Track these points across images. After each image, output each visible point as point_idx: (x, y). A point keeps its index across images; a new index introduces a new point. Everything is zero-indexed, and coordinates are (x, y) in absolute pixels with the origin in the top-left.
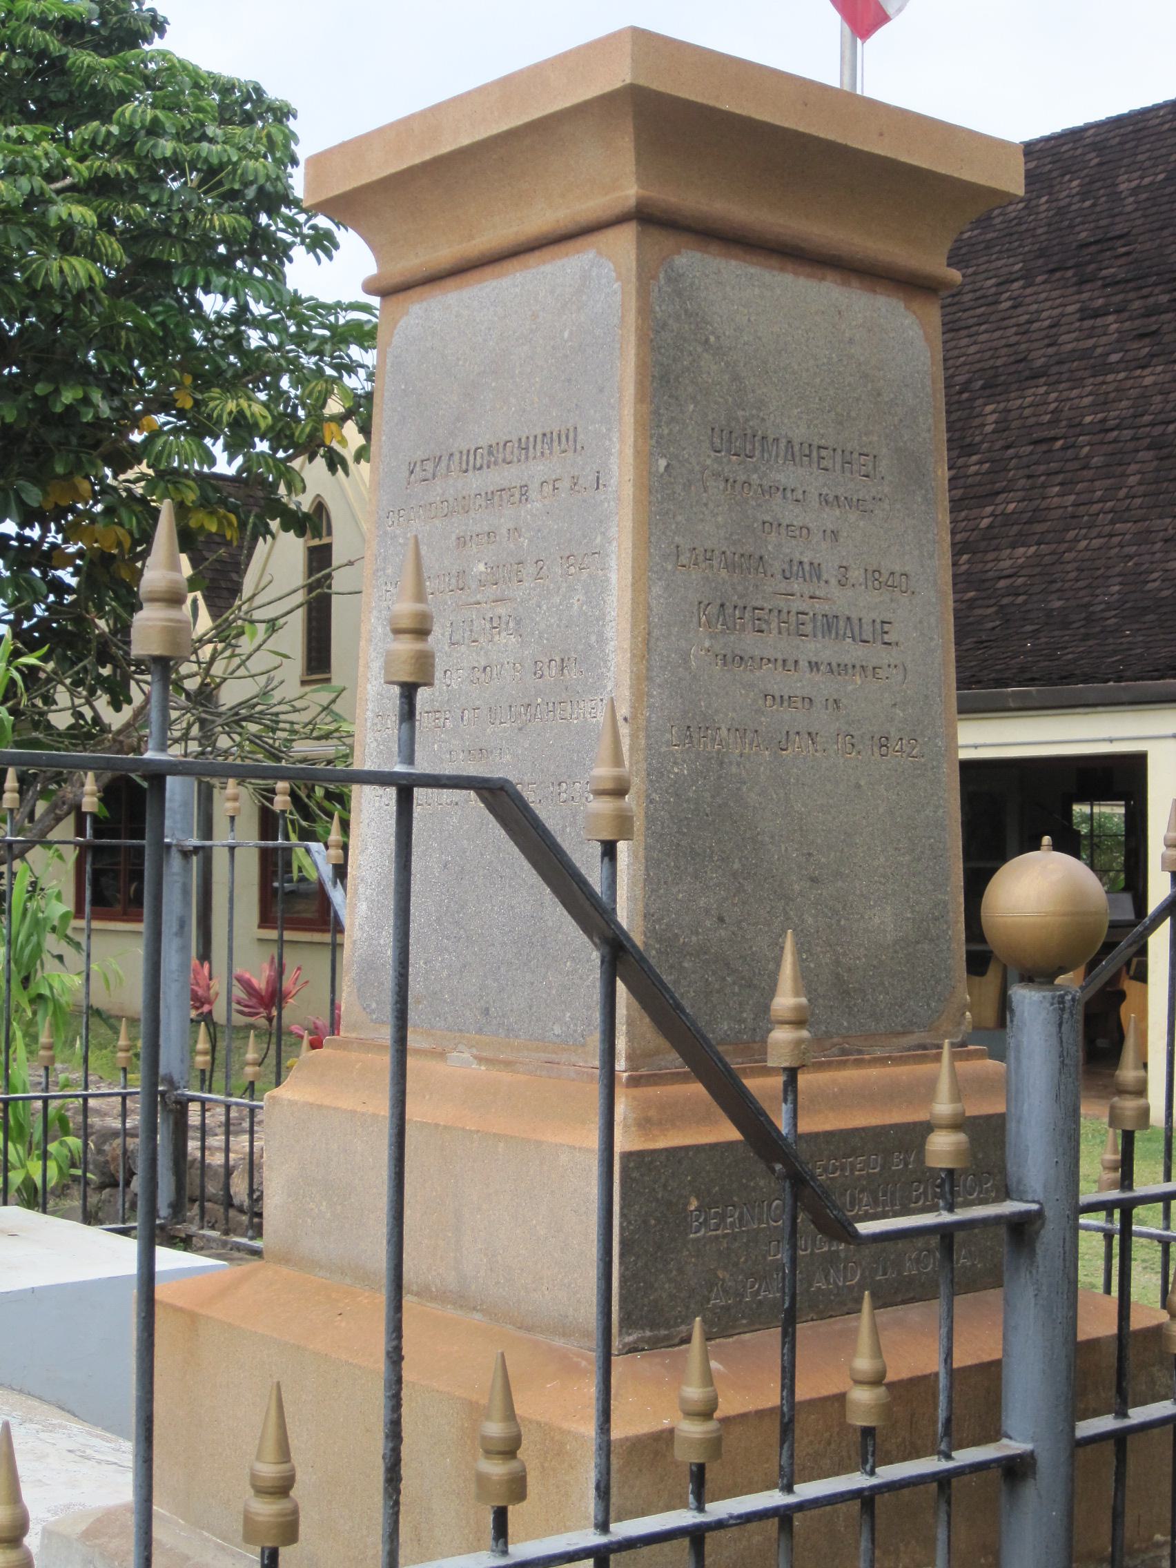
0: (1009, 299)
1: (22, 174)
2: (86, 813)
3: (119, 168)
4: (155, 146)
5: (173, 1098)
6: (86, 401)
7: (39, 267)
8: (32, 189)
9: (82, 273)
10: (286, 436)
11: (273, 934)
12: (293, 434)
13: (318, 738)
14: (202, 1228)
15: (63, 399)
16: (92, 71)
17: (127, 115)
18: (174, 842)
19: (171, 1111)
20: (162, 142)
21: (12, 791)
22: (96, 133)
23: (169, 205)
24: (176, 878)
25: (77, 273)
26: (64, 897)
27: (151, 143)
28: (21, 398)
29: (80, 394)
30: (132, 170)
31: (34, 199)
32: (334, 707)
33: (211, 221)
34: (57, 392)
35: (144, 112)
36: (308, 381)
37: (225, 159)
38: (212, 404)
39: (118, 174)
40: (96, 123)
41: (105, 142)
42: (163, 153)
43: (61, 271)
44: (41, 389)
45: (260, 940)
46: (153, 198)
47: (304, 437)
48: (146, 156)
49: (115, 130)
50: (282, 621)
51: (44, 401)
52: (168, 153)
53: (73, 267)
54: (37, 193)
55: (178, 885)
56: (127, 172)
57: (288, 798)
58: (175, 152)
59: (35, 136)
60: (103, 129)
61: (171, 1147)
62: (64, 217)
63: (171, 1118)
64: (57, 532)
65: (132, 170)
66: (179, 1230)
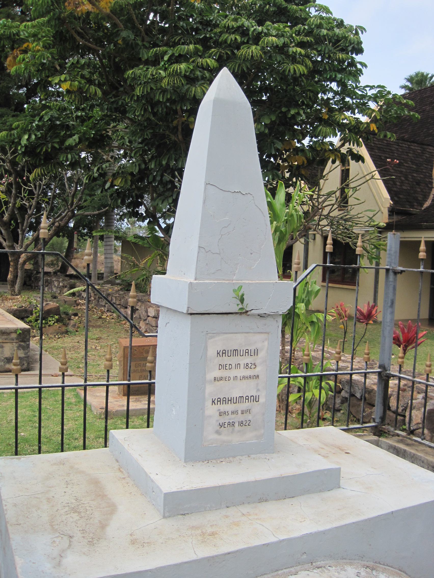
0: (383, 142)
1: (281, 37)
2: (327, 252)
3: (309, 39)
4: (320, 31)
5: (385, 374)
6: (298, 114)
7: (287, 67)
8: (284, 42)
9: (301, 70)
10: (357, 128)
11: (325, 284)
12: (359, 128)
13: (371, 227)
14: (396, 430)
15: (291, 113)
16: (296, 11)
17: (312, 21)
18: (391, 268)
19: (383, 380)
20: (323, 30)
21: (423, 251)
22: (300, 28)
23: (324, 51)
24: (391, 283)
25: (299, 69)
26: (317, 283)
27: (319, 30)
28: (277, 113)
29: (297, 111)
30: (312, 40)
31: (285, 45)
32: (373, 218)
33: (339, 55)
34: (289, 111)
35: (317, 20)
36: (364, 110)
37: (344, 36)
38: (336, 116)
39: (308, 41)
40: (300, 25)
41: (303, 32)
42: (323, 34)
43: (294, 68)
44: (284, 109)
45: (322, 286)
46: (319, 49)
47: (364, 128)
48: (318, 35)
49: (306, 27)
50: (358, 188)
51: (285, 114)
52: (325, 34)
53: (298, 67)
54: (286, 43)
55: (392, 286)
56: (311, 41)
57: (332, 246)
58: (327, 34)
59: (283, 27)
60: (303, 28)
61: (382, 394)
62: (295, 51)
63: (383, 383)
64: (280, 160)
65: (312, 40)
66: (385, 429)
